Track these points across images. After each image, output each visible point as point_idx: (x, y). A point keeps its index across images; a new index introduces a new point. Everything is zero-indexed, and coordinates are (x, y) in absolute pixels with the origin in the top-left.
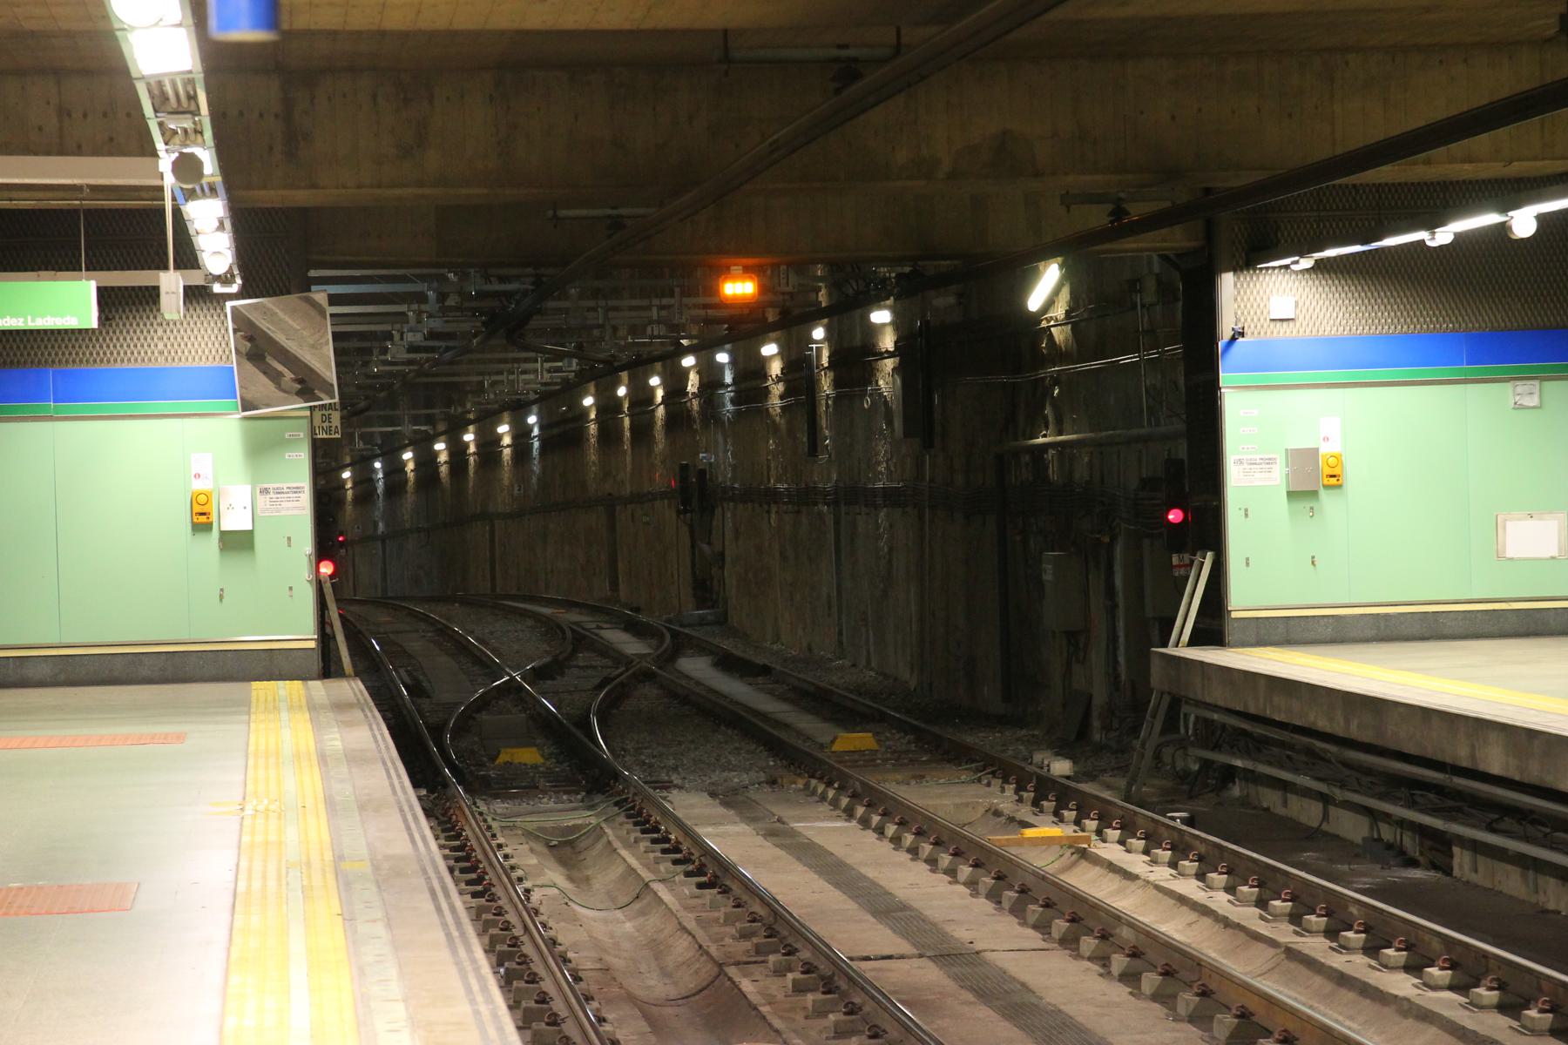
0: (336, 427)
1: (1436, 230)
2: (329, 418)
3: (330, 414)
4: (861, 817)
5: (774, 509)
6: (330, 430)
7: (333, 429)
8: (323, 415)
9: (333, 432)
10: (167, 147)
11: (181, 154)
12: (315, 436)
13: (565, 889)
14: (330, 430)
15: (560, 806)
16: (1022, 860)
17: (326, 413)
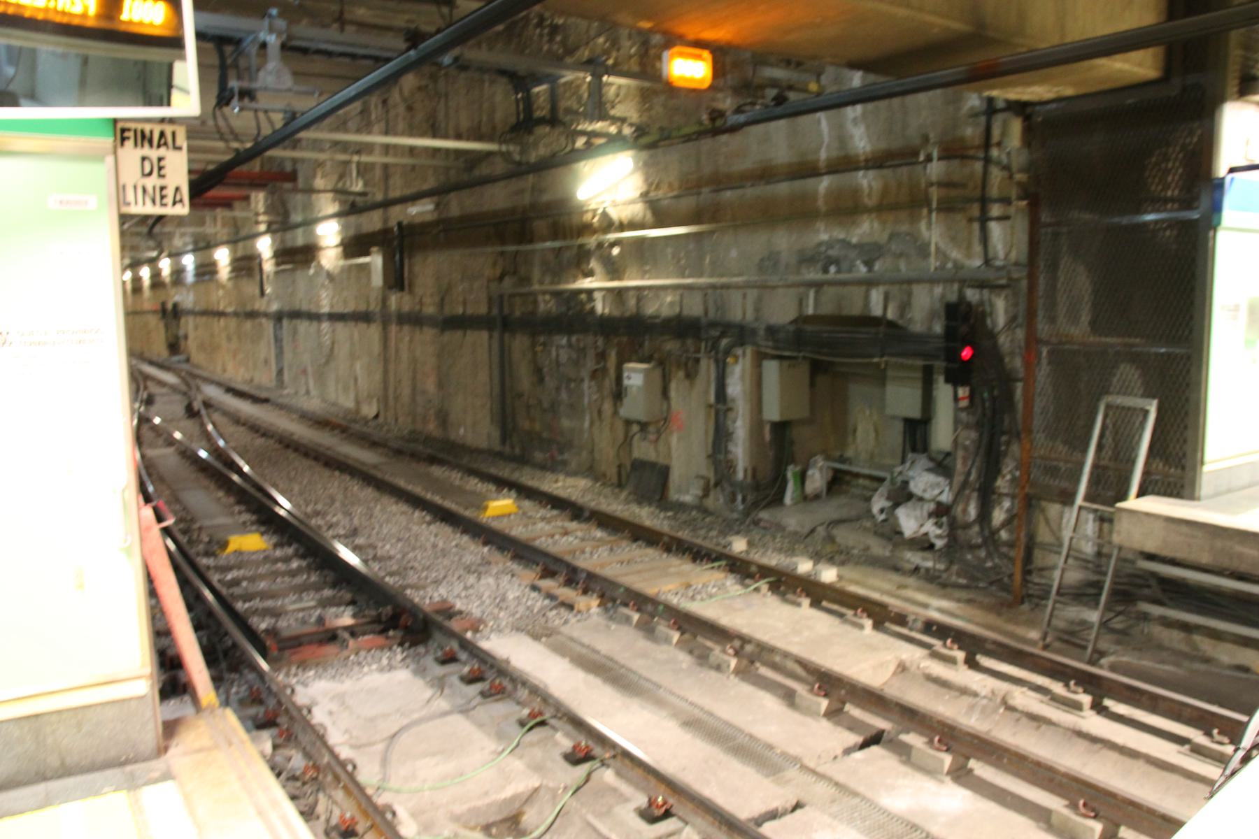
0: (177, 189)
1: (1016, 501)
2: (160, 168)
3: (160, 159)
4: (735, 668)
5: (779, 535)
6: (162, 197)
7: (170, 192)
8: (144, 159)
9: (169, 200)
10: (762, 333)
11: (949, 773)
12: (125, 210)
13: (478, 570)
14: (162, 197)
15: (139, 126)
16: (462, 19)
17: (154, 154)
